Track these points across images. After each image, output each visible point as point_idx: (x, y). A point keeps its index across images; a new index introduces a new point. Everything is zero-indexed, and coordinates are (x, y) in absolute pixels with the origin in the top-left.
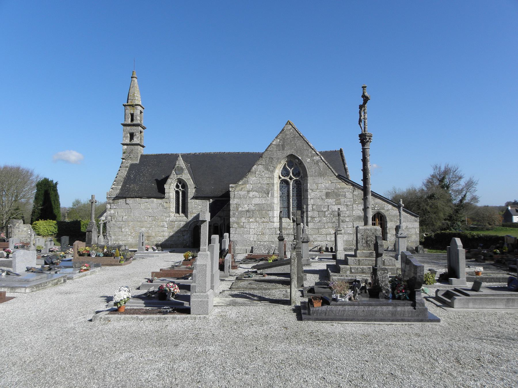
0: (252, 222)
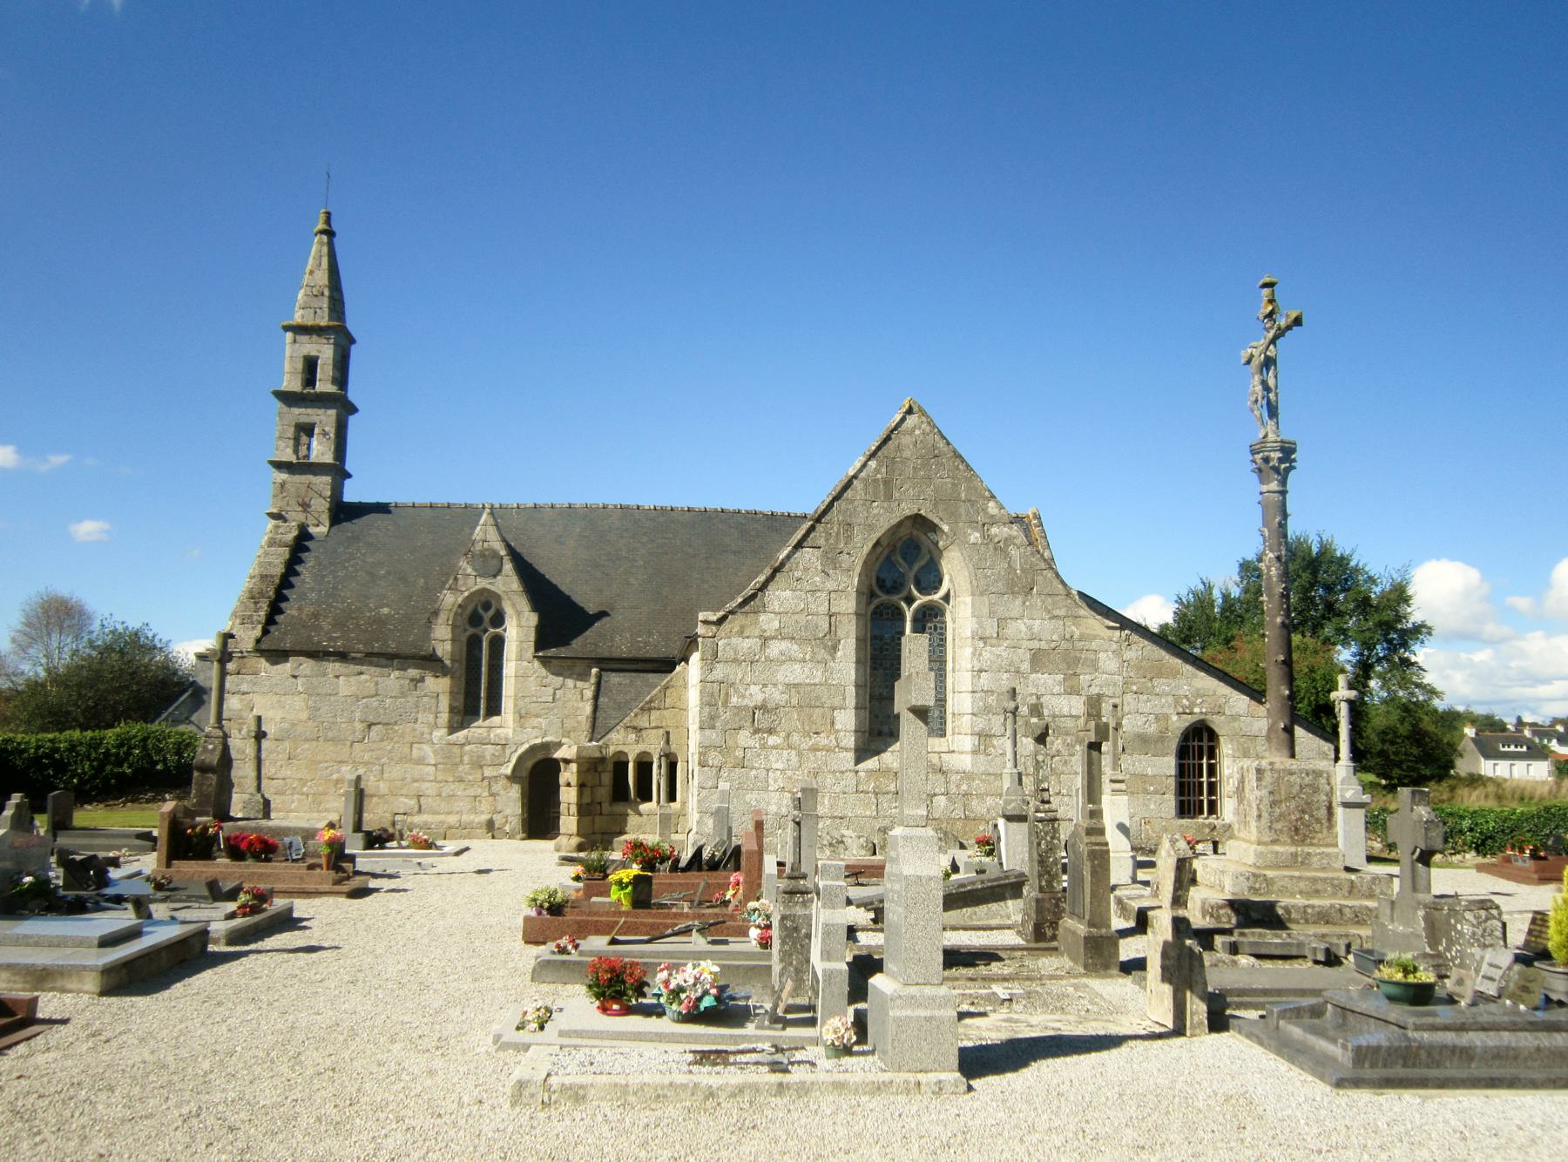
0: (775, 747)
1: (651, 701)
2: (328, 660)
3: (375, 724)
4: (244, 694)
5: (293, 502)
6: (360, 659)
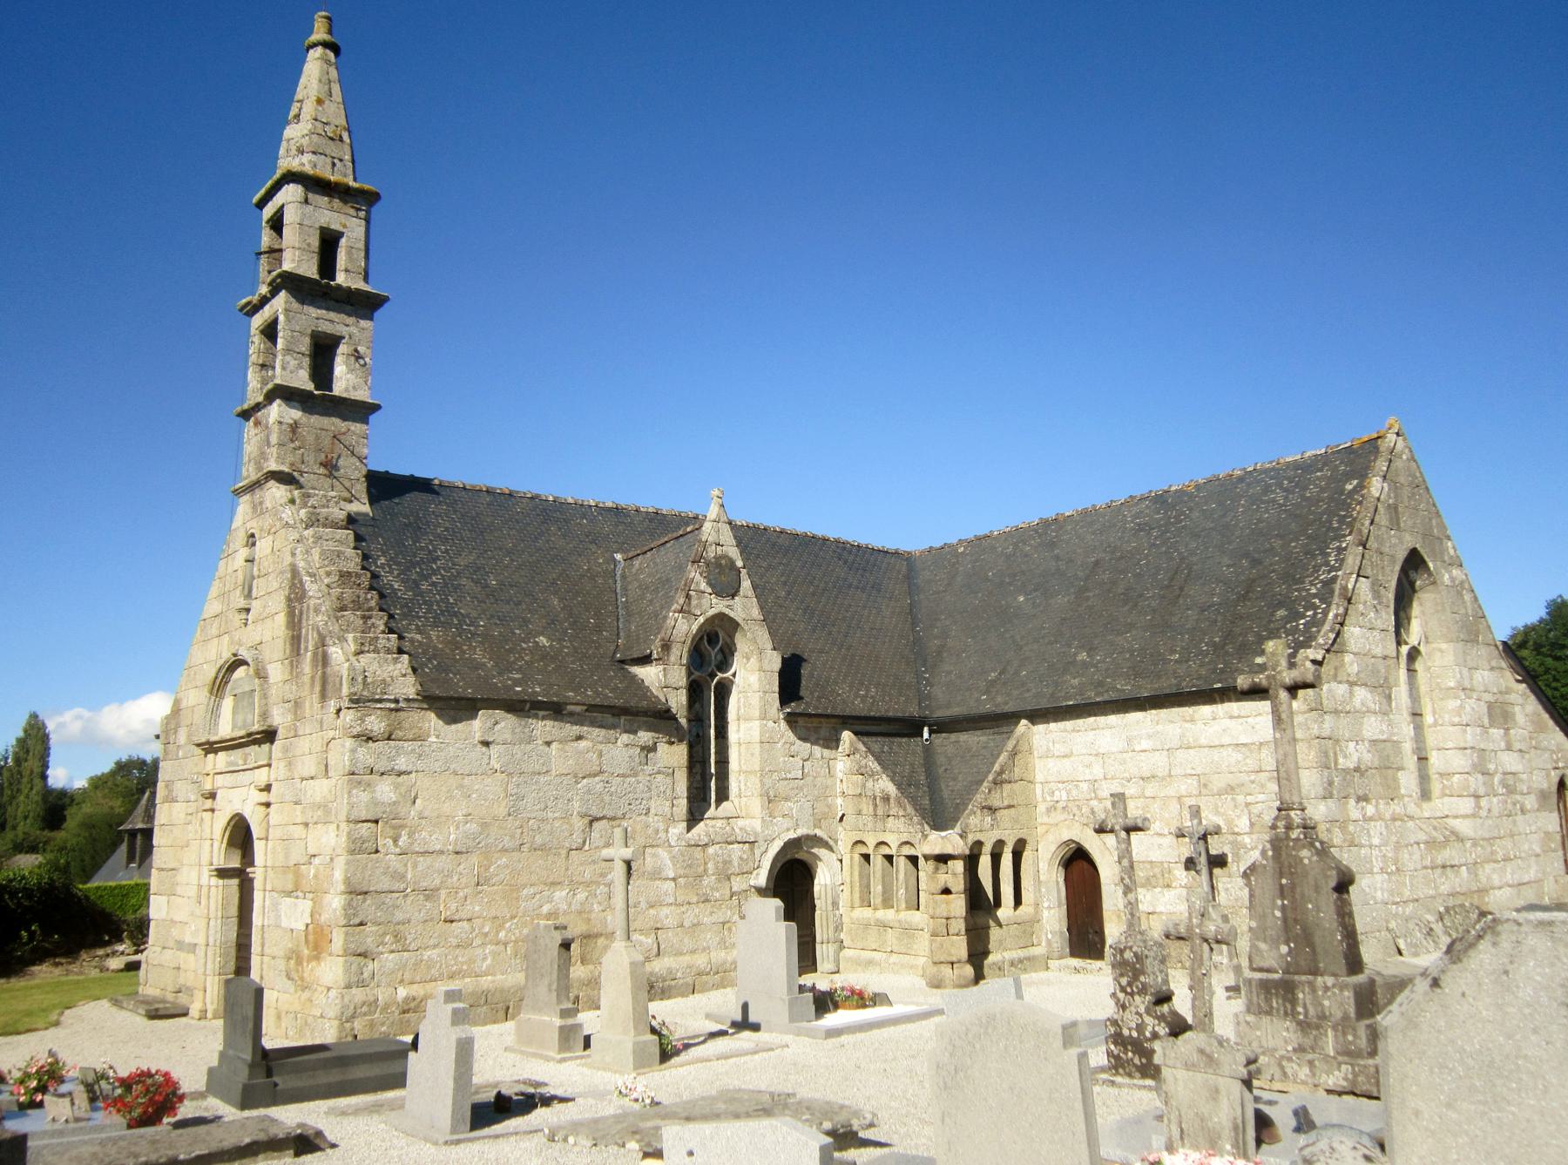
1: (1001, 772)
2: (536, 717)
3: (597, 819)
4: (400, 774)
5: (310, 458)
6: (579, 714)
